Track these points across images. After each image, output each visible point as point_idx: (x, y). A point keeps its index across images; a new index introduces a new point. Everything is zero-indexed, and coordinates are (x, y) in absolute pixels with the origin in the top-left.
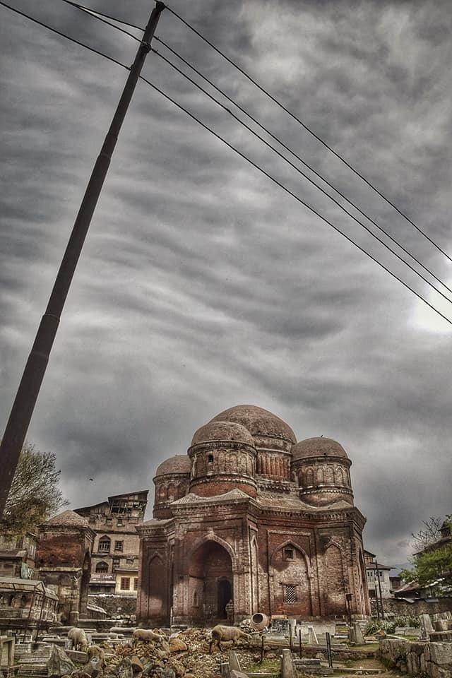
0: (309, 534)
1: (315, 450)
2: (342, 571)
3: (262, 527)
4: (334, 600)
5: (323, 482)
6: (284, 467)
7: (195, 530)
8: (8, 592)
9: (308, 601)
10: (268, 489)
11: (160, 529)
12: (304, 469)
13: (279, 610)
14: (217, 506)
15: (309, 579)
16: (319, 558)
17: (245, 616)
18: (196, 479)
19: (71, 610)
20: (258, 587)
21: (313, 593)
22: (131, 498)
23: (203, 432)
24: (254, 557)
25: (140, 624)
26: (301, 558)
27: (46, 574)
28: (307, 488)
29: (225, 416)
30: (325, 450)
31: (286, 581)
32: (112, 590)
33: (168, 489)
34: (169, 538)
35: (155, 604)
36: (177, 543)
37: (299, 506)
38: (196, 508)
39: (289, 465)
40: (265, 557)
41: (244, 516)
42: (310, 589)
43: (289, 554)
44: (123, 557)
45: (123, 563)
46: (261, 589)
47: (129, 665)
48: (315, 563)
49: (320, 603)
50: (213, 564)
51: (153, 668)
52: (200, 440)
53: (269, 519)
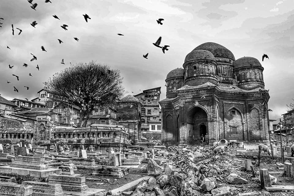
0: (243, 103)
1: (246, 63)
2: (259, 121)
3: (221, 100)
4: (255, 133)
5: (250, 79)
6: (230, 71)
7: (189, 102)
8: (107, 131)
9: (242, 134)
10: (223, 82)
11: (170, 103)
12: (240, 73)
13: (229, 138)
14: (200, 90)
15: (243, 124)
16: (248, 115)
17: (214, 141)
18: (188, 78)
19: (135, 139)
20: (219, 128)
21: (245, 130)
22: (153, 91)
23: (189, 56)
24: (217, 114)
25: (163, 144)
26: (239, 114)
27: (122, 123)
28: (241, 81)
29: (200, 48)
30: (251, 63)
31: (232, 125)
32: (148, 130)
33: (173, 84)
34: (175, 106)
35: (170, 136)
36: (181, 108)
37: (238, 90)
38: (189, 92)
39: (232, 71)
40: (222, 114)
41: (213, 95)
42: (243, 129)
43: (234, 112)
44: (152, 116)
45: (151, 119)
46: (221, 128)
47: (193, 168)
48: (246, 117)
49: (248, 135)
50: (197, 118)
51: (201, 169)
52: (189, 59)
53: (224, 96)
